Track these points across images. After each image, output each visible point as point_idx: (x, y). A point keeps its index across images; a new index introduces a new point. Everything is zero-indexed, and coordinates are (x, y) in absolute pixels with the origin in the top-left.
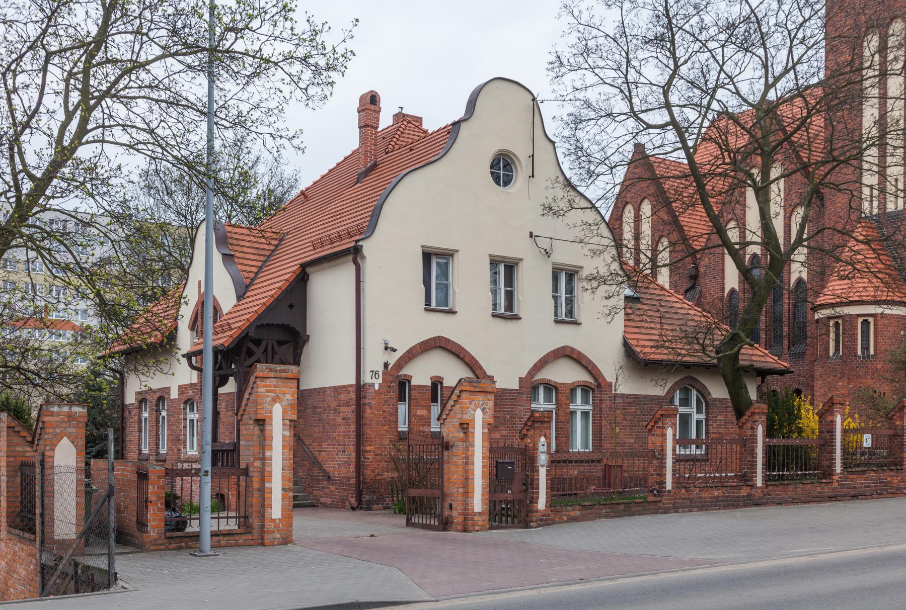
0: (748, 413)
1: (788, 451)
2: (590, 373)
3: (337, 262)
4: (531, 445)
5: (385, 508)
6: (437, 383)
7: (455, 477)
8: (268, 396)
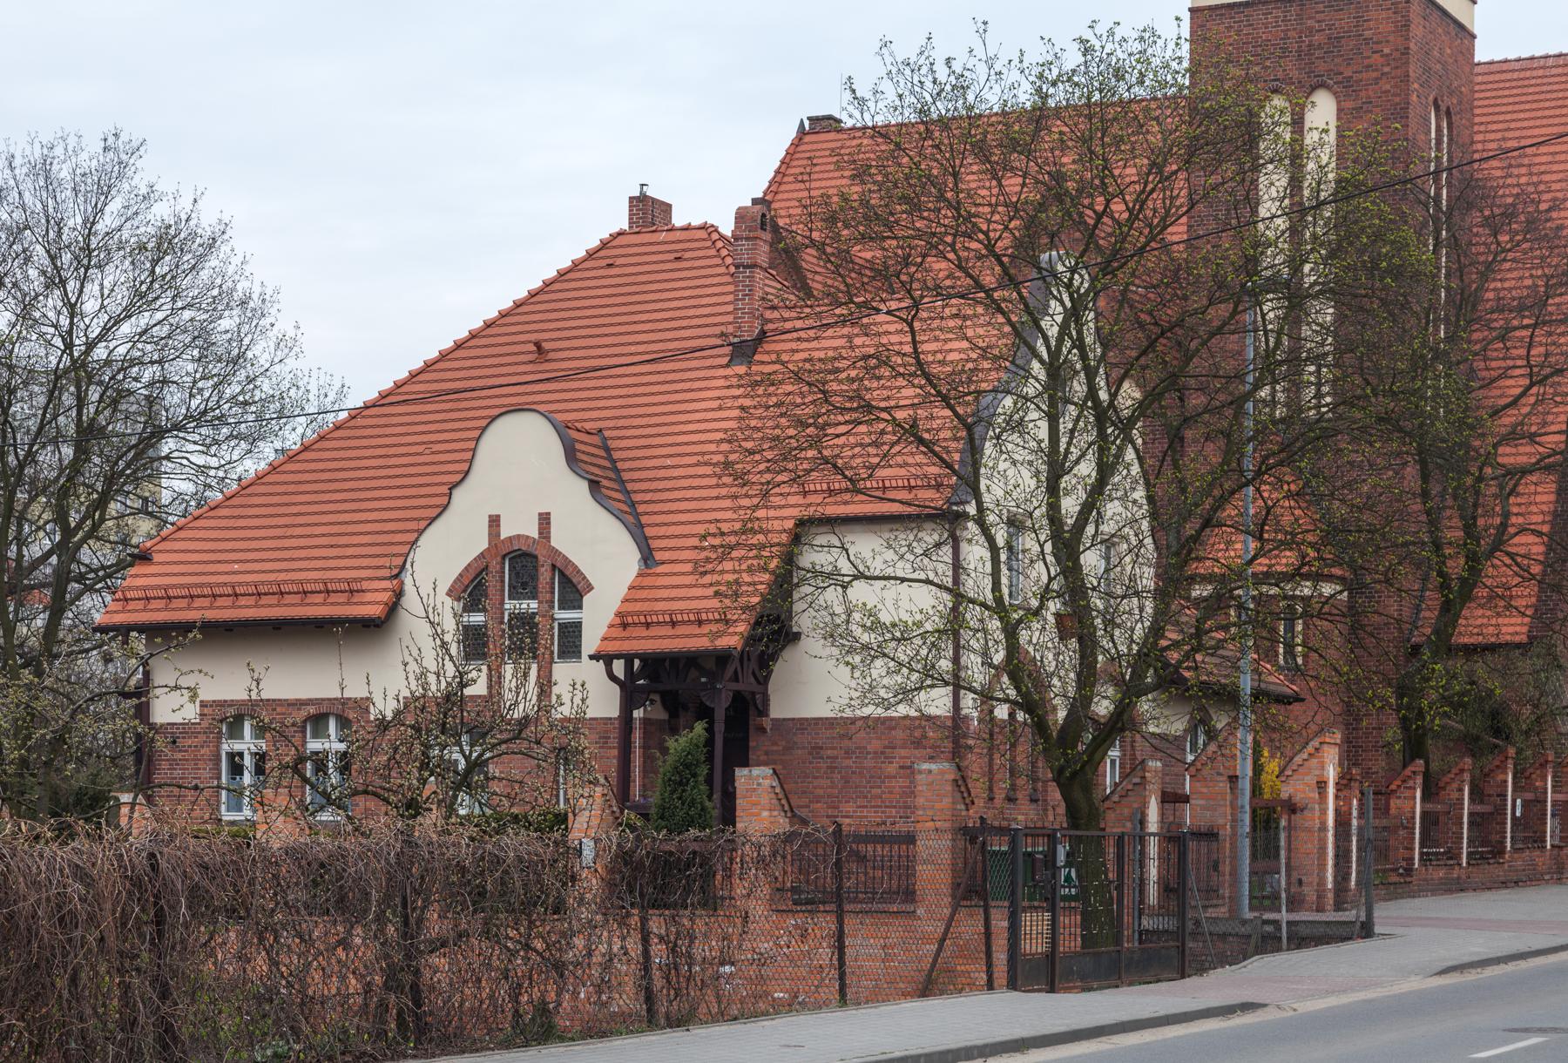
1: (1487, 823)
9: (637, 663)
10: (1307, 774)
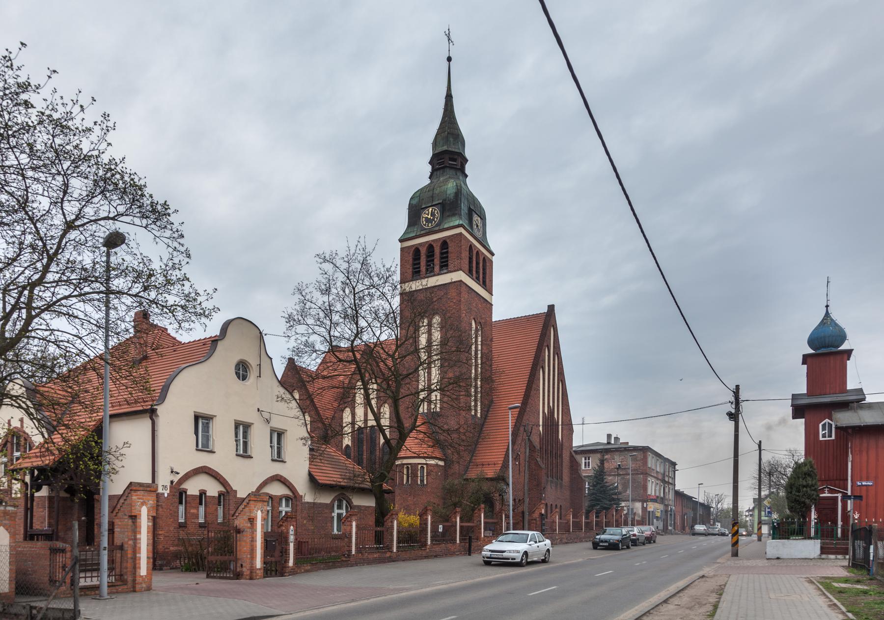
0: (389, 514)
2: (291, 490)
3: (136, 416)
4: (285, 531)
5: (171, 569)
6: (203, 493)
7: (245, 549)
8: (138, 502)
9: (36, 472)
10: (244, 515)
